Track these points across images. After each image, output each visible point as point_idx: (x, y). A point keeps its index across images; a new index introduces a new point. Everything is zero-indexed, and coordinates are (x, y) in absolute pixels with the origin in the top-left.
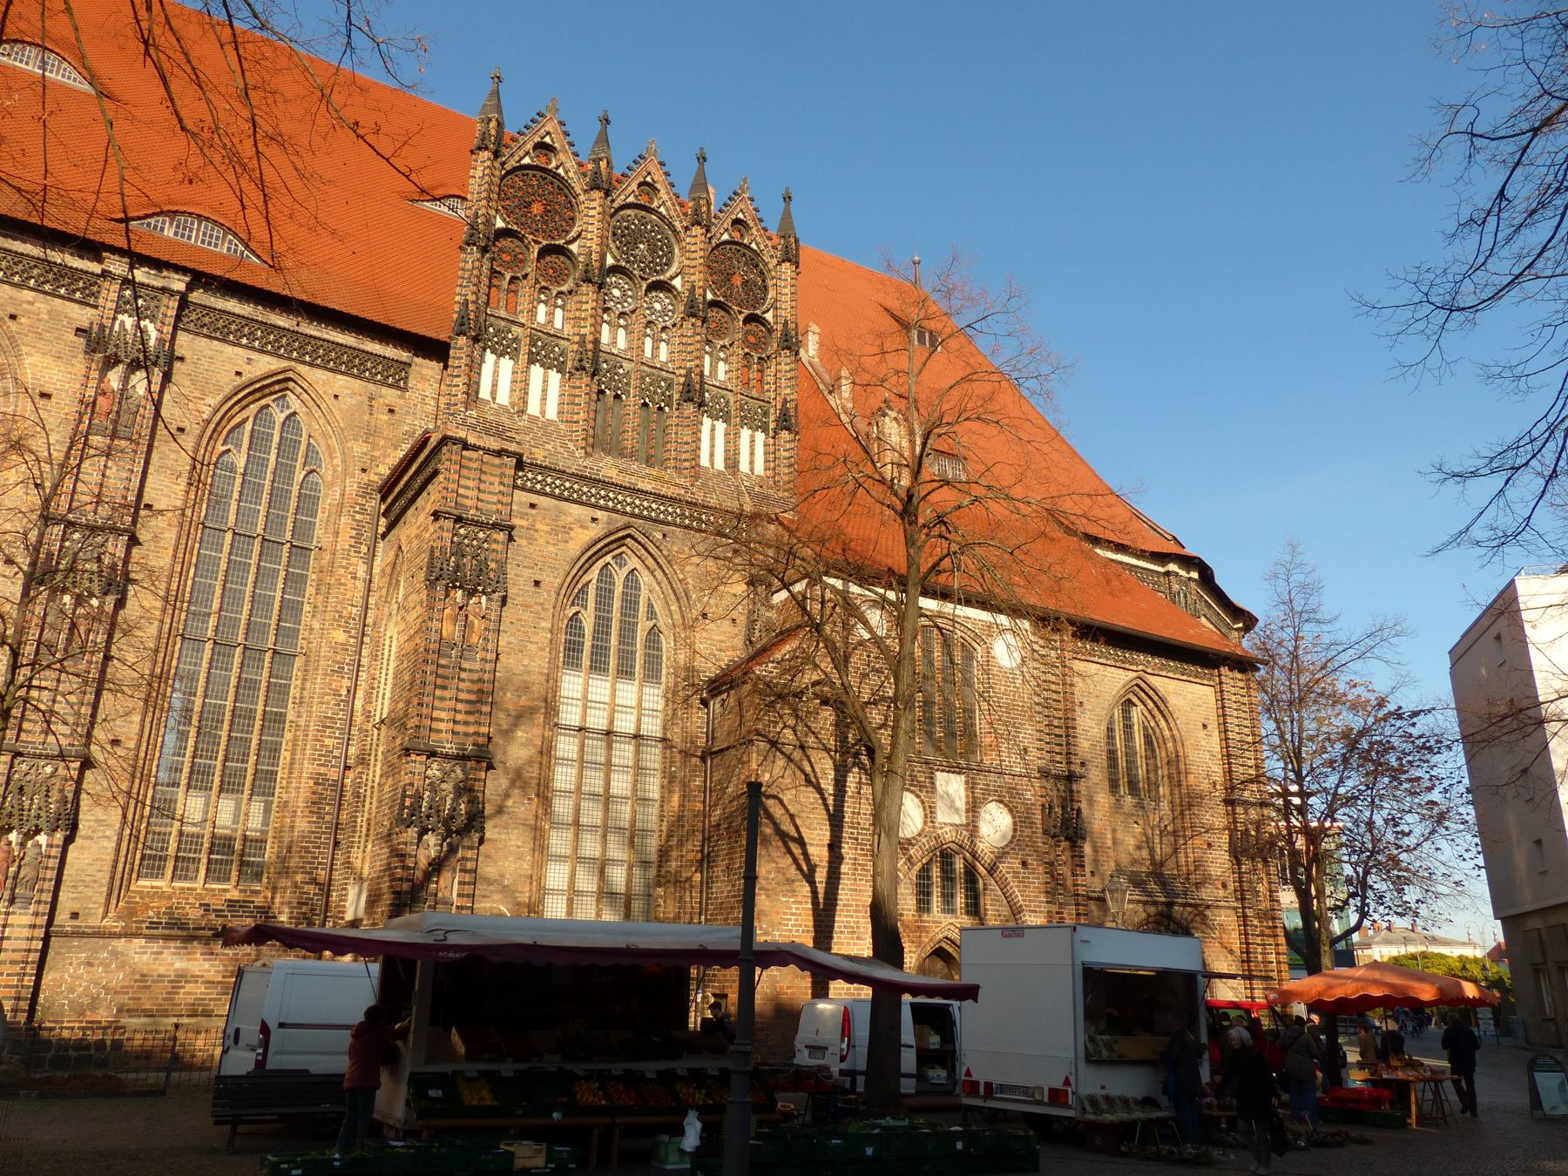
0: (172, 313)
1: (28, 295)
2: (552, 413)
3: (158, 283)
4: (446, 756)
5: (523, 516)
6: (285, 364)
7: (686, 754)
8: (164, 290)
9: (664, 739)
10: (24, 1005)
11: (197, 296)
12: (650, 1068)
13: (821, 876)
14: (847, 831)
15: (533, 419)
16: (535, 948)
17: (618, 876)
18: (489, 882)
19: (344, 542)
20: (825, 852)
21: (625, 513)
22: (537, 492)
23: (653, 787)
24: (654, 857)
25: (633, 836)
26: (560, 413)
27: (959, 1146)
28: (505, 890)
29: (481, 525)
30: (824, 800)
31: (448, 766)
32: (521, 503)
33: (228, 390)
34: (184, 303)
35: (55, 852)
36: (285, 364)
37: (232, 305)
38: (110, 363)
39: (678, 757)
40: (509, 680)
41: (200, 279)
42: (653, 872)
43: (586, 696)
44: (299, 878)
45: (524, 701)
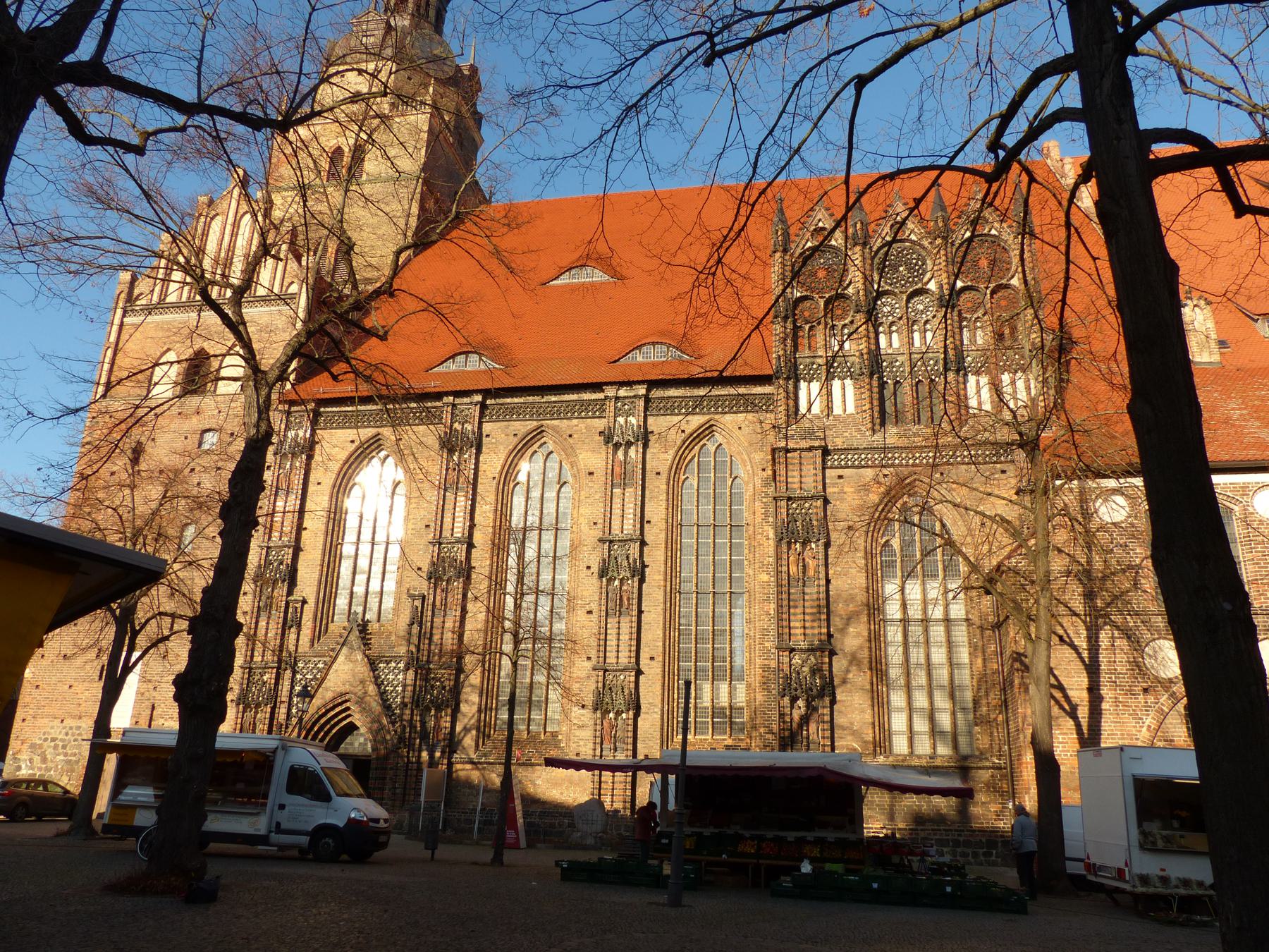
0: (642, 408)
1: (575, 421)
2: (851, 409)
3: (632, 394)
4: (802, 650)
5: (834, 485)
6: (707, 417)
7: (982, 628)
8: (635, 396)
9: (967, 620)
10: (628, 805)
11: (656, 393)
12: (791, 836)
13: (1083, 713)
14: (1104, 678)
15: (837, 418)
16: (731, 768)
17: (945, 720)
18: (843, 728)
19: (759, 518)
20: (1085, 694)
21: (907, 466)
22: (842, 467)
23: (964, 655)
24: (971, 705)
25: (953, 692)
26: (857, 407)
27: (949, 889)
28: (854, 733)
29: (805, 499)
30: (1079, 654)
31: (804, 656)
32: (832, 477)
33: (679, 443)
34: (647, 400)
35: (631, 722)
36: (707, 417)
37: (673, 392)
38: (617, 446)
39: (978, 632)
40: (839, 595)
41: (652, 384)
42: (971, 716)
43: (906, 596)
44: (762, 730)
45: (851, 607)
